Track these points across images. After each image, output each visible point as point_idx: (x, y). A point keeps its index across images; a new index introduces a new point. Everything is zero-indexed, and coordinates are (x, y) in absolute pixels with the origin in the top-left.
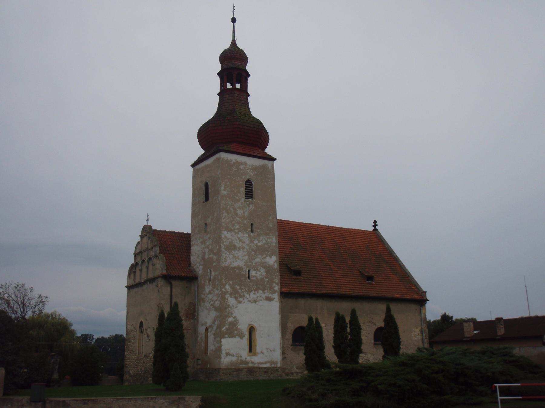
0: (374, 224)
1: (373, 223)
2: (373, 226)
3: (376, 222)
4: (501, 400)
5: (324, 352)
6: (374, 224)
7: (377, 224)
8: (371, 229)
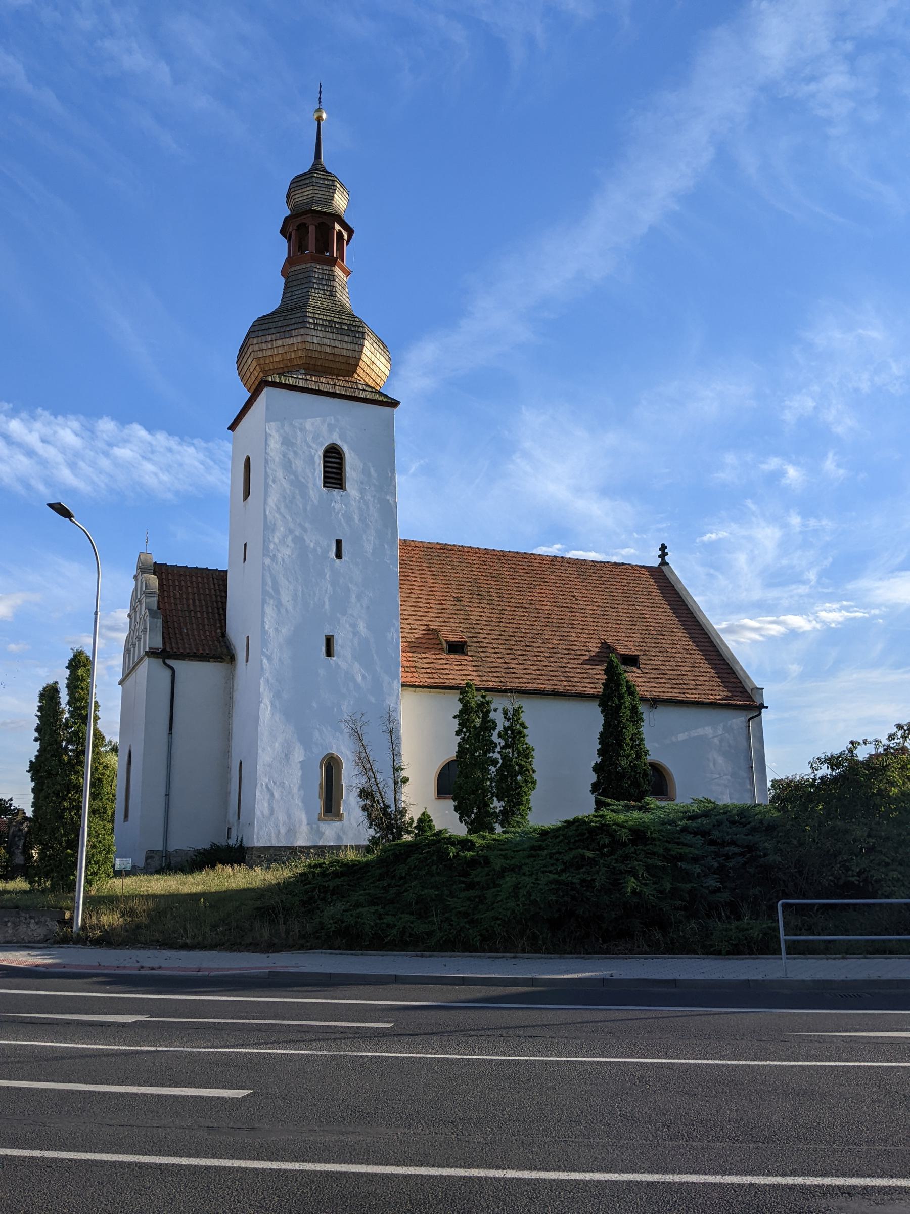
0: (660, 553)
1: (660, 549)
2: (660, 557)
3: (666, 548)
4: (786, 941)
5: (38, 751)
6: (660, 553)
7: (666, 551)
8: (655, 562)
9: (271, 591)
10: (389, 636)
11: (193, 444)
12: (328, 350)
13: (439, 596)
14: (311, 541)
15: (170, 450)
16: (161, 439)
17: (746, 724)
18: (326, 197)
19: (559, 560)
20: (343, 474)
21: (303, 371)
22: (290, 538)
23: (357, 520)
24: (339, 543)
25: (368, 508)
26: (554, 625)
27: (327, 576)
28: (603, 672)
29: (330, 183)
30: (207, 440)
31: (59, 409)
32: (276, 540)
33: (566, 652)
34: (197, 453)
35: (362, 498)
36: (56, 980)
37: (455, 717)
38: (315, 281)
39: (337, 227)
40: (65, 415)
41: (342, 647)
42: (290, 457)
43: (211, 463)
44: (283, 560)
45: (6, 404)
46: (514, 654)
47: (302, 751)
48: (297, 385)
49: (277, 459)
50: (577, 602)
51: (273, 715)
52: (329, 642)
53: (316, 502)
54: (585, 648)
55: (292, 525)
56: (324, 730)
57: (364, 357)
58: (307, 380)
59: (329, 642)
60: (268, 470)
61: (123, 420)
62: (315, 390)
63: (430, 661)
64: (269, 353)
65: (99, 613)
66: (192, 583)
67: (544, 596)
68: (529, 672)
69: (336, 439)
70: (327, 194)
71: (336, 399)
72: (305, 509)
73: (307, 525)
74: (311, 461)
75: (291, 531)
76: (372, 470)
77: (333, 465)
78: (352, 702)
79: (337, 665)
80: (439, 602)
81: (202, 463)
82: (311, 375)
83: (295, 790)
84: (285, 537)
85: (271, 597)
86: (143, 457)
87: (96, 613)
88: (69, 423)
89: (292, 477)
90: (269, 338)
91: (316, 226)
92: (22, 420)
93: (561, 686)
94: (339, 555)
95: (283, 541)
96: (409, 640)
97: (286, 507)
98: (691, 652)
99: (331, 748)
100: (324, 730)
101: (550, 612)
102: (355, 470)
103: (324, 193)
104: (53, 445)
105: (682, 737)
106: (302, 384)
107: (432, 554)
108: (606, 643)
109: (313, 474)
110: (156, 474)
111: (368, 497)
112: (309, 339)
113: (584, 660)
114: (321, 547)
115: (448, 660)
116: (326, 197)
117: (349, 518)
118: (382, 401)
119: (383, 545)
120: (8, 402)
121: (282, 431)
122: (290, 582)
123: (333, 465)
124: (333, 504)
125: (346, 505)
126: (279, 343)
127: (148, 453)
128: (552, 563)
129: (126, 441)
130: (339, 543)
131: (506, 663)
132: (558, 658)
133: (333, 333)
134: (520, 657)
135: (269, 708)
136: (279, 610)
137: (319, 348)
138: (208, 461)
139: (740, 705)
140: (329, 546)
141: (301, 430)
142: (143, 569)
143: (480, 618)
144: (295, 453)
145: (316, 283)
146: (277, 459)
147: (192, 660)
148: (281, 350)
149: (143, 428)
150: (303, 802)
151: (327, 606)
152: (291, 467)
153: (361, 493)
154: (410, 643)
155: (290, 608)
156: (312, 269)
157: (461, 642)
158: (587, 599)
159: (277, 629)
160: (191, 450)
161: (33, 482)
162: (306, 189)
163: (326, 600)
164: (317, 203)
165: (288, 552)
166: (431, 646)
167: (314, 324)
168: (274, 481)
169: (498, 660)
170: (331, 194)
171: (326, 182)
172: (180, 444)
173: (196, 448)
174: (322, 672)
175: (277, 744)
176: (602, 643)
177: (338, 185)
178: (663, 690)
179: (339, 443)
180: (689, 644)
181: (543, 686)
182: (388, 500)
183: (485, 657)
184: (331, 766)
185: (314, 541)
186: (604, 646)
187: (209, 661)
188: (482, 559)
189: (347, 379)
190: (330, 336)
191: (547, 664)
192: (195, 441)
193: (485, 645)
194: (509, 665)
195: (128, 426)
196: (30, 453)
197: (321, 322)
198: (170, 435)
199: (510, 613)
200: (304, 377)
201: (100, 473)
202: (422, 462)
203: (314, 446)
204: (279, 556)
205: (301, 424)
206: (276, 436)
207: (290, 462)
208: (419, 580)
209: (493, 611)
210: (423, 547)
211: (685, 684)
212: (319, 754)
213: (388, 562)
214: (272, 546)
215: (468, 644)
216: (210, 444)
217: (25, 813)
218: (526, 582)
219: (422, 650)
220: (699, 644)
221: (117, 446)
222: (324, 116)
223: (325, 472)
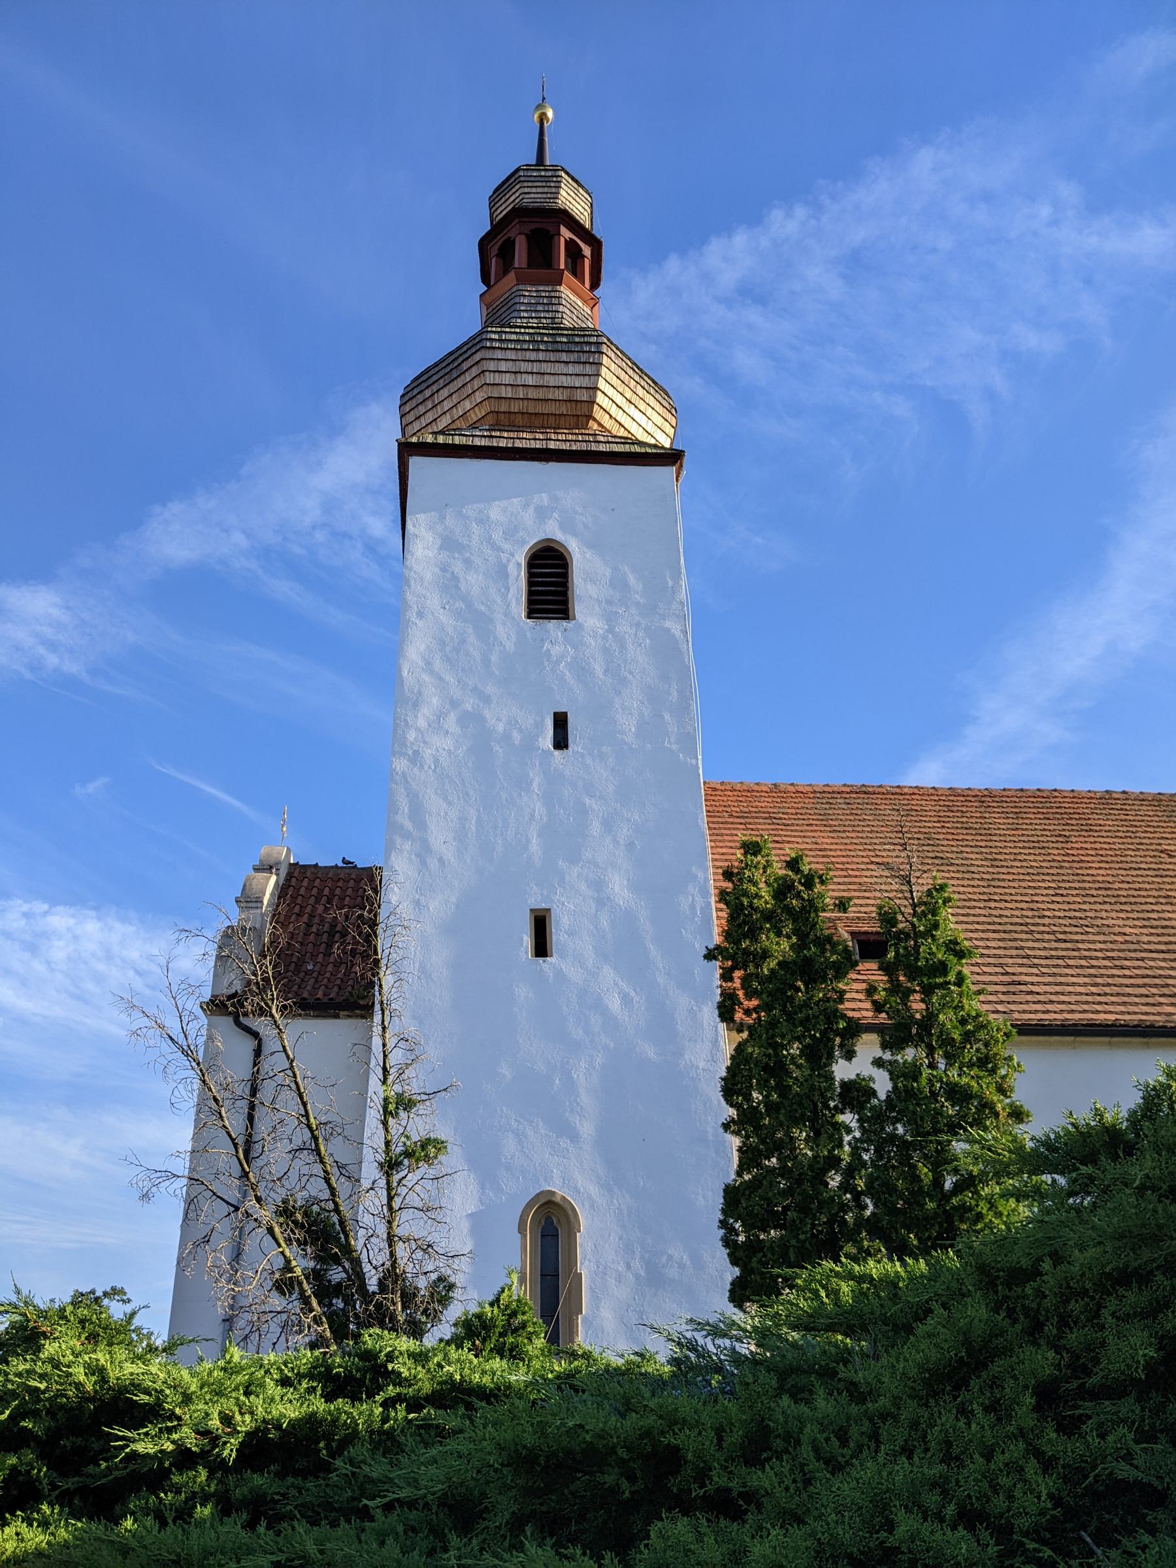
14: (499, 720)
18: (545, 196)
20: (569, 593)
22: (452, 717)
23: (599, 669)
25: (623, 647)
26: (1123, 900)
27: (535, 785)
32: (422, 723)
33: (1163, 947)
35: (610, 630)
37: (710, 956)
39: (566, 233)
41: (571, 933)
42: (456, 571)
44: (436, 761)
46: (1028, 957)
52: (541, 924)
53: (510, 646)
55: (456, 692)
56: (530, 1133)
59: (541, 924)
67: (1092, 852)
68: (1071, 989)
69: (553, 531)
70: (546, 190)
71: (552, 464)
72: (486, 662)
73: (490, 689)
74: (502, 573)
75: (454, 704)
76: (632, 579)
78: (599, 1060)
79: (560, 975)
80: (844, 873)
84: (441, 715)
85: (407, 836)
91: (527, 235)
93: (1159, 1014)
94: (561, 742)
95: (437, 724)
100: (530, 1133)
101: (1110, 879)
103: (539, 190)
109: (504, 597)
114: (520, 730)
116: (545, 196)
117: (581, 670)
118: (647, 453)
119: (662, 717)
122: (450, 804)
124: (547, 645)
125: (575, 647)
128: (1103, 801)
131: (1007, 973)
134: (1043, 962)
136: (423, 863)
140: (539, 726)
144: (468, 563)
151: (535, 845)
152: (457, 587)
155: (450, 855)
156: (518, 293)
159: (417, 903)
162: (510, 193)
165: (448, 743)
167: (500, 340)
169: (986, 969)
170: (553, 190)
174: (522, 992)
177: (563, 174)
179: (559, 536)
181: (1112, 1017)
182: (669, 630)
185: (505, 720)
187: (337, 1016)
188: (942, 803)
190: (533, 356)
191: (1115, 972)
194: (1015, 978)
199: (1011, 884)
203: (506, 546)
204: (427, 753)
206: (429, 537)
207: (454, 578)
209: (971, 883)
210: (815, 792)
213: (674, 747)
214: (411, 735)
218: (1048, 833)
222: (550, 114)
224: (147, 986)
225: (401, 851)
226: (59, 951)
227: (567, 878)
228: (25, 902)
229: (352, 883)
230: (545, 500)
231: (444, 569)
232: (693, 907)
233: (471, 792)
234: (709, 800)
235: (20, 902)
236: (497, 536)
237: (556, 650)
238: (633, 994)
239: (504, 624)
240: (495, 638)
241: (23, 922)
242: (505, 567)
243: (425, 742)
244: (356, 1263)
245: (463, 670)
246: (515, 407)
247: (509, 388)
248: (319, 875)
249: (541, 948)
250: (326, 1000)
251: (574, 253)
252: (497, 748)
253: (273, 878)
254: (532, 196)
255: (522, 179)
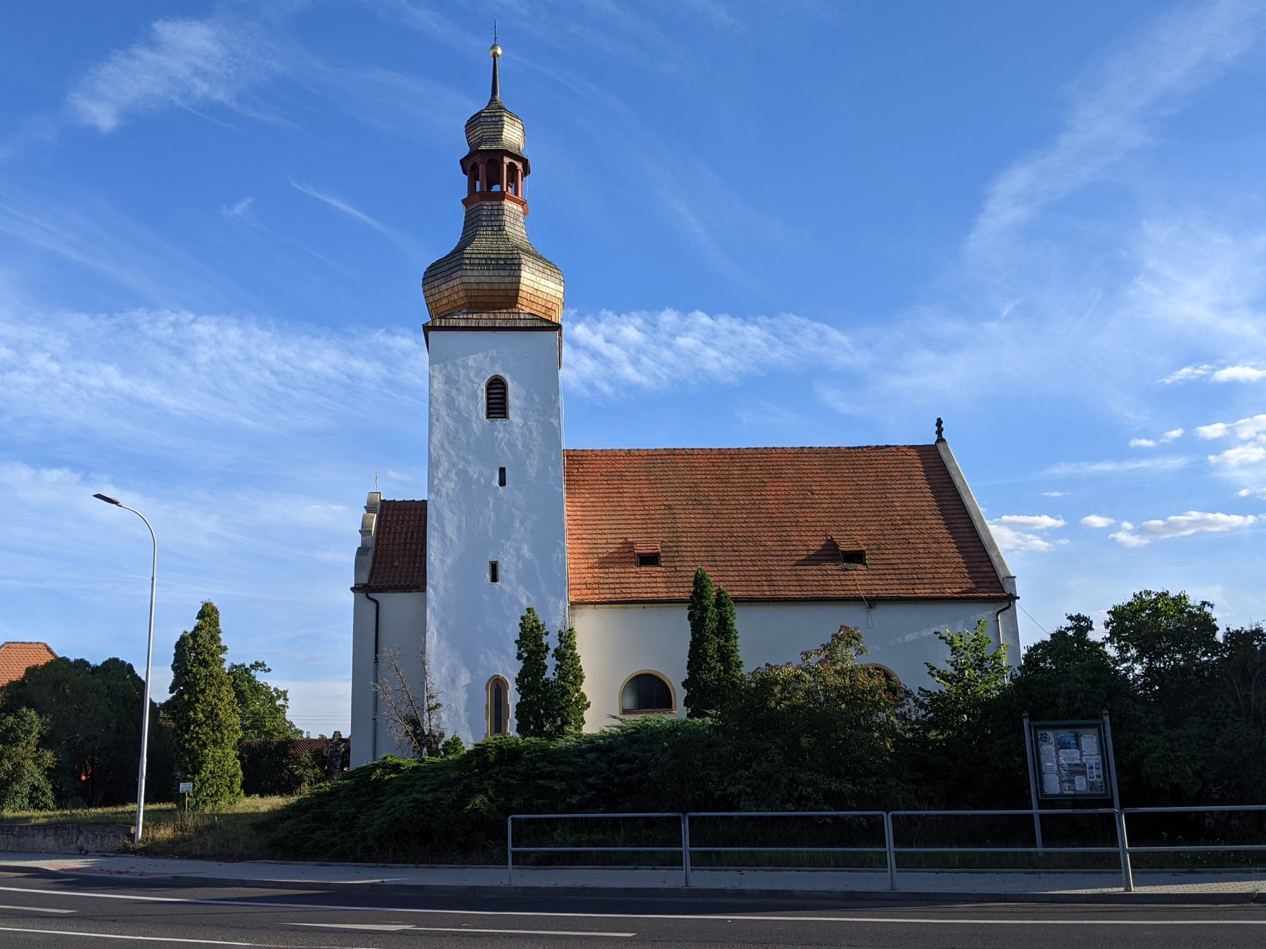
8: (931, 439)
9: (436, 525)
10: (555, 556)
11: (756, 323)
12: (486, 287)
13: (649, 506)
14: (475, 472)
15: (733, 332)
16: (724, 322)
17: (994, 619)
19: (805, 451)
21: (465, 311)
24: (502, 471)
25: (531, 433)
27: (491, 504)
28: (691, 585)
29: (497, 119)
30: (771, 316)
31: (622, 308)
32: (440, 476)
34: (761, 330)
35: (525, 424)
36: (712, 886)
38: (484, 219)
39: (507, 160)
40: (628, 313)
42: (453, 395)
43: (775, 339)
44: (447, 494)
45: (571, 310)
46: (715, 561)
47: (468, 674)
48: (457, 325)
49: (441, 399)
50: (812, 497)
51: (439, 642)
52: (494, 567)
53: (478, 434)
54: (804, 548)
55: (455, 459)
57: (522, 287)
58: (468, 319)
59: (494, 567)
60: (432, 410)
61: (685, 309)
62: (475, 327)
63: (617, 575)
64: (437, 297)
65: (155, 579)
66: (415, 516)
70: (496, 130)
73: (470, 457)
74: (474, 395)
75: (454, 465)
76: (535, 397)
77: (497, 396)
79: (501, 589)
81: (766, 341)
82: (473, 313)
83: (462, 711)
84: (449, 471)
86: (704, 343)
87: (153, 579)
88: (632, 320)
89: (455, 413)
90: (436, 283)
92: (587, 323)
95: (447, 477)
96: (601, 556)
97: (450, 442)
98: (941, 540)
99: (497, 671)
102: (517, 398)
103: (493, 130)
104: (617, 345)
105: (909, 637)
106: (462, 323)
107: (655, 461)
108: (832, 539)
109: (476, 408)
110: (718, 359)
111: (531, 423)
112: (466, 280)
113: (798, 560)
114: (484, 477)
115: (637, 573)
117: (512, 445)
118: (543, 327)
119: (548, 469)
120: (573, 308)
121: (445, 372)
122: (454, 514)
123: (497, 396)
124: (496, 433)
126: (444, 287)
127: (710, 338)
129: (688, 329)
130: (502, 471)
132: (767, 561)
133: (489, 269)
135: (436, 635)
137: (477, 287)
138: (771, 337)
139: (983, 598)
141: (463, 367)
142: (369, 509)
143: (688, 525)
144: (459, 390)
145: (485, 221)
146: (441, 399)
147: (395, 592)
148: (446, 294)
149: (705, 314)
150: (469, 723)
151: (490, 533)
153: (524, 419)
154: (601, 558)
155: (455, 538)
157: (653, 554)
158: (826, 492)
159: (442, 560)
160: (755, 329)
161: (597, 383)
162: (476, 130)
163: (490, 527)
164: (486, 141)
165: (452, 485)
166: (622, 560)
167: (470, 264)
168: (437, 420)
170: (500, 130)
171: (494, 119)
172: (742, 325)
173: (759, 326)
175: (443, 670)
176: (827, 540)
178: (887, 587)
179: (502, 374)
180: (942, 532)
182: (552, 423)
183: (680, 566)
184: (498, 687)
186: (830, 543)
189: (510, 311)
190: (487, 273)
192: (759, 319)
193: (685, 553)
195: (690, 315)
196: (595, 355)
197: (477, 261)
198: (732, 317)
200: (465, 316)
201: (662, 365)
202: (1017, 301)
203: (477, 380)
204: (444, 490)
205: (464, 362)
206: (440, 377)
207: (453, 399)
208: (632, 491)
211: (918, 578)
212: (485, 676)
214: (436, 482)
215: (661, 555)
216: (775, 320)
217: (341, 735)
219: (612, 565)
220: (953, 531)
221: (680, 335)
222: (499, 51)
223: (488, 404)
224: (280, 384)
225: (434, 537)
226: (204, 355)
227: (505, 547)
228: (173, 312)
229: (413, 512)
230: (495, 353)
231: (448, 394)
232: (558, 558)
233: (463, 508)
234: (570, 489)
235: (169, 312)
236: (472, 374)
237: (501, 435)
238: (531, 596)
239: (476, 422)
240: (472, 430)
241: (171, 330)
242: (476, 392)
243: (442, 485)
244: (423, 730)
245: (458, 448)
246: (479, 300)
247: (476, 291)
248: (397, 507)
249: (494, 578)
250: (405, 586)
251: (512, 168)
252: (474, 486)
253: (376, 515)
254: (488, 134)
255: (482, 124)
